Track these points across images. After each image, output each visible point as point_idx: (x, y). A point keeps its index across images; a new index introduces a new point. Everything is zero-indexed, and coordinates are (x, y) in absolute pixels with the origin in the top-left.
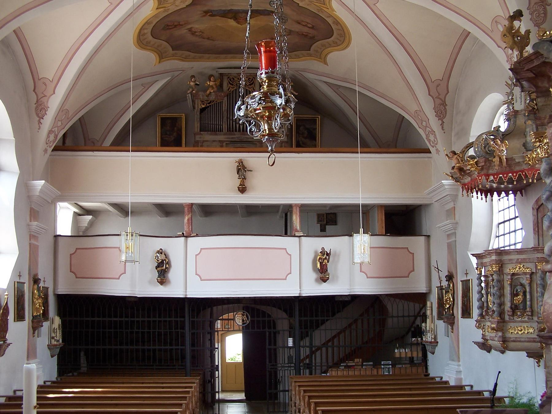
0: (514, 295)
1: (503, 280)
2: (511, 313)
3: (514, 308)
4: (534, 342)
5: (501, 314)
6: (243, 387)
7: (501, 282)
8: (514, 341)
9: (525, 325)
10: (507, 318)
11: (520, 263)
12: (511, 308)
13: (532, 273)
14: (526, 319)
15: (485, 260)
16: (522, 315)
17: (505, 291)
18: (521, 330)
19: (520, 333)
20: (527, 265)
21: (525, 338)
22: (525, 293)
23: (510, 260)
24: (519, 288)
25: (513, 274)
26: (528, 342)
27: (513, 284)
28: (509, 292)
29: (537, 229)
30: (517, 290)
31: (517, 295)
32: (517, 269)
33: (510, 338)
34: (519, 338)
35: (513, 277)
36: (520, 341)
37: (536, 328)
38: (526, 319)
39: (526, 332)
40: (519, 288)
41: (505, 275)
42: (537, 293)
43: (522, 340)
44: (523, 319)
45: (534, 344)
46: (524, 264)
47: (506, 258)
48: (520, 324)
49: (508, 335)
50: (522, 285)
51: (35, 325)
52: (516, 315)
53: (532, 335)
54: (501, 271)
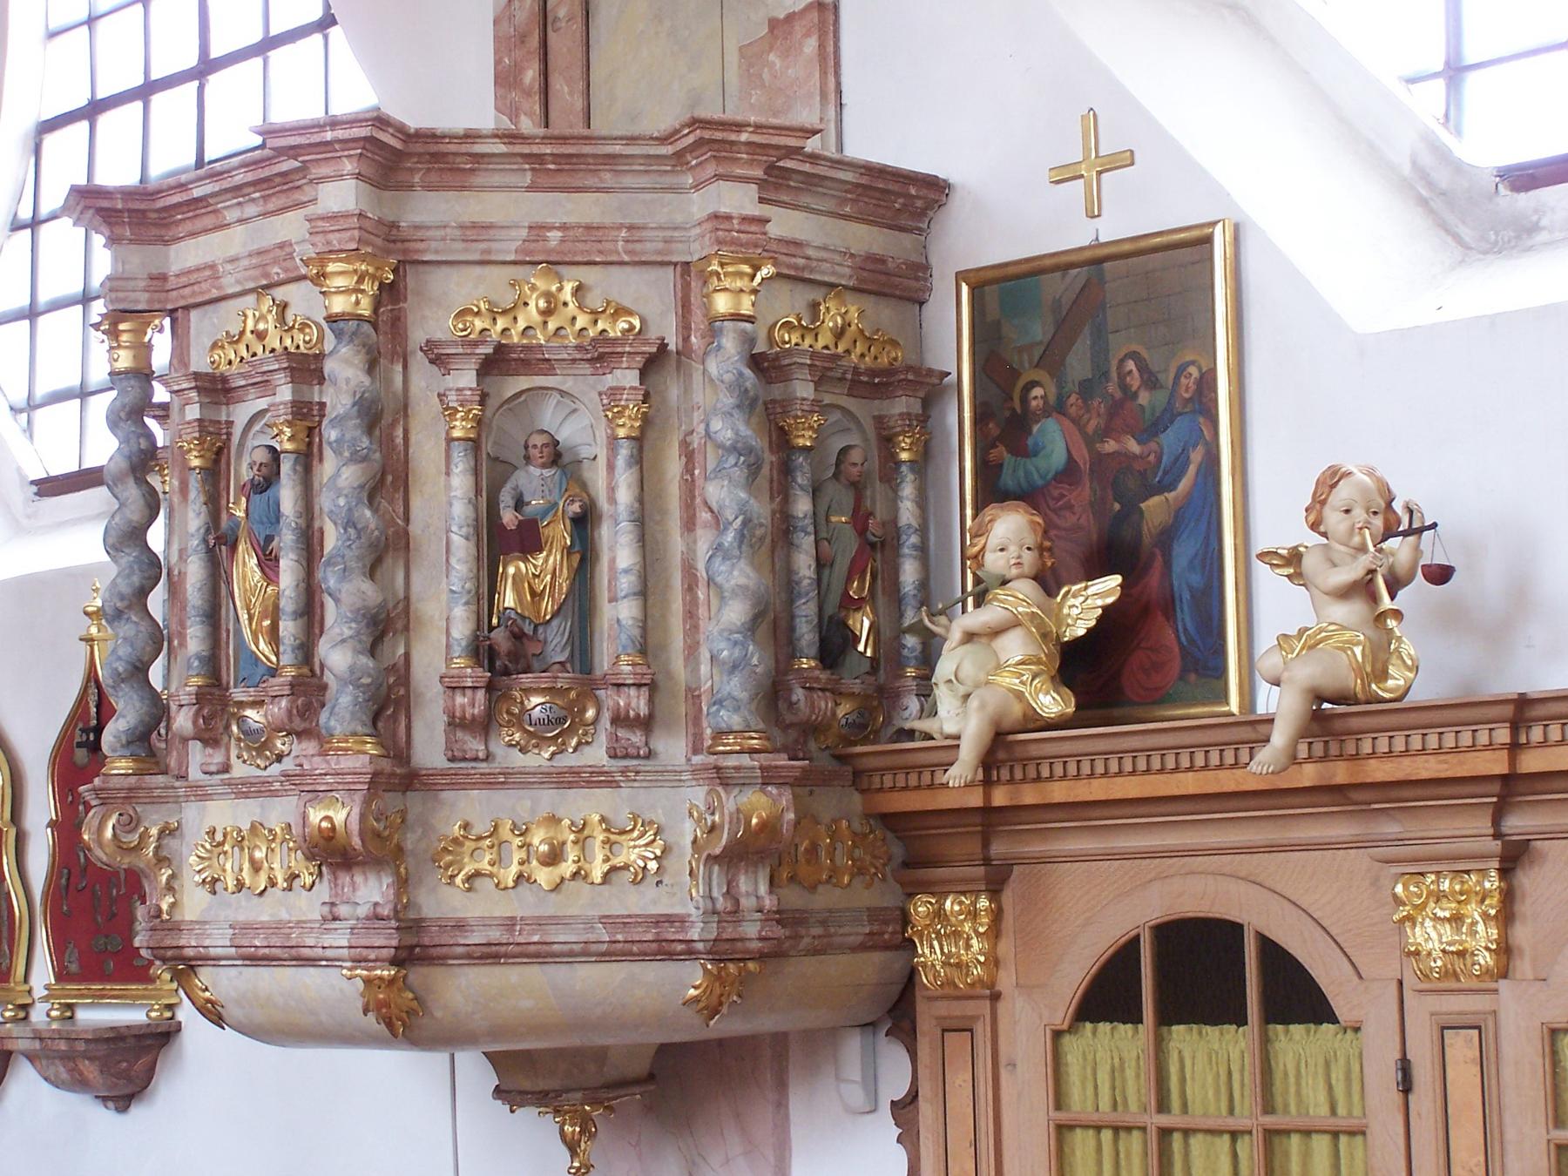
0: (503, 540)
1: (404, 408)
2: (472, 704)
3: (501, 656)
4: (663, 951)
5: (388, 704)
6: (86, 465)
7: (381, 419)
8: (491, 955)
9: (589, 805)
10: (429, 746)
11: (554, 265)
12: (481, 651)
13: (655, 362)
14: (596, 755)
15: (186, 255)
16: (565, 724)
17: (416, 503)
18: (554, 857)
19: (544, 876)
20: (607, 284)
21: (589, 924)
22: (584, 522)
23: (477, 230)
24: (534, 482)
25: (499, 361)
26: (611, 955)
27: (488, 447)
28: (460, 511)
29: (531, 75)
30: (519, 504)
31: (528, 540)
32: (531, 314)
33: (461, 926)
34: (540, 923)
35: (492, 382)
36: (542, 955)
37: (687, 831)
38: (596, 755)
39: (597, 871)
40: (534, 482)
41: (419, 362)
42: (689, 525)
43: (562, 936)
44: (569, 760)
45: (653, 974)
46: (589, 275)
47: (431, 210)
48: (548, 799)
49: (443, 901)
50: (556, 456)
51: (1507, 865)
52: (518, 721)
53: (649, 889)
54: (384, 329)
